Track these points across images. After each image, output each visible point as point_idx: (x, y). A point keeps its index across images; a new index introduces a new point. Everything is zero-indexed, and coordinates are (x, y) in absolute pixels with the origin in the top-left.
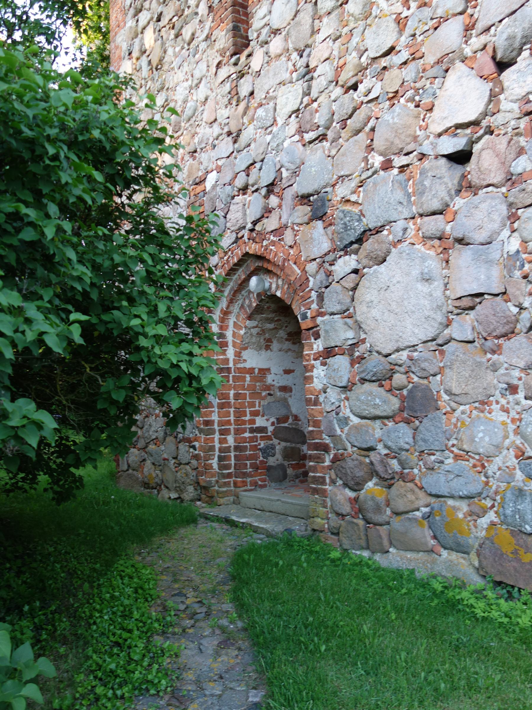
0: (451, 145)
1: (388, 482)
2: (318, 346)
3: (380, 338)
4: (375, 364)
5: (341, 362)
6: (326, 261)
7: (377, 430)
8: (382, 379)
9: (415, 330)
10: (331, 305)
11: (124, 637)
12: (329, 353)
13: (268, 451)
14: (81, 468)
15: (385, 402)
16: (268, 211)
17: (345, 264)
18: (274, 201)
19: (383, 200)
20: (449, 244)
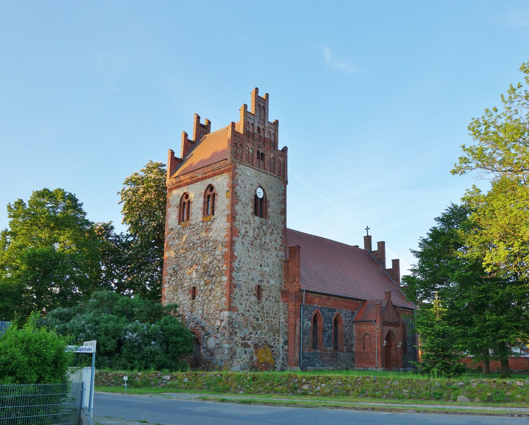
1: (209, 363)
5: (205, 349)
6: (204, 336)
7: (208, 357)
8: (209, 351)
9: (213, 346)
11: (484, 237)
12: (203, 348)
13: (193, 362)
16: (196, 326)
17: (206, 337)
19: (210, 331)
20: (216, 338)
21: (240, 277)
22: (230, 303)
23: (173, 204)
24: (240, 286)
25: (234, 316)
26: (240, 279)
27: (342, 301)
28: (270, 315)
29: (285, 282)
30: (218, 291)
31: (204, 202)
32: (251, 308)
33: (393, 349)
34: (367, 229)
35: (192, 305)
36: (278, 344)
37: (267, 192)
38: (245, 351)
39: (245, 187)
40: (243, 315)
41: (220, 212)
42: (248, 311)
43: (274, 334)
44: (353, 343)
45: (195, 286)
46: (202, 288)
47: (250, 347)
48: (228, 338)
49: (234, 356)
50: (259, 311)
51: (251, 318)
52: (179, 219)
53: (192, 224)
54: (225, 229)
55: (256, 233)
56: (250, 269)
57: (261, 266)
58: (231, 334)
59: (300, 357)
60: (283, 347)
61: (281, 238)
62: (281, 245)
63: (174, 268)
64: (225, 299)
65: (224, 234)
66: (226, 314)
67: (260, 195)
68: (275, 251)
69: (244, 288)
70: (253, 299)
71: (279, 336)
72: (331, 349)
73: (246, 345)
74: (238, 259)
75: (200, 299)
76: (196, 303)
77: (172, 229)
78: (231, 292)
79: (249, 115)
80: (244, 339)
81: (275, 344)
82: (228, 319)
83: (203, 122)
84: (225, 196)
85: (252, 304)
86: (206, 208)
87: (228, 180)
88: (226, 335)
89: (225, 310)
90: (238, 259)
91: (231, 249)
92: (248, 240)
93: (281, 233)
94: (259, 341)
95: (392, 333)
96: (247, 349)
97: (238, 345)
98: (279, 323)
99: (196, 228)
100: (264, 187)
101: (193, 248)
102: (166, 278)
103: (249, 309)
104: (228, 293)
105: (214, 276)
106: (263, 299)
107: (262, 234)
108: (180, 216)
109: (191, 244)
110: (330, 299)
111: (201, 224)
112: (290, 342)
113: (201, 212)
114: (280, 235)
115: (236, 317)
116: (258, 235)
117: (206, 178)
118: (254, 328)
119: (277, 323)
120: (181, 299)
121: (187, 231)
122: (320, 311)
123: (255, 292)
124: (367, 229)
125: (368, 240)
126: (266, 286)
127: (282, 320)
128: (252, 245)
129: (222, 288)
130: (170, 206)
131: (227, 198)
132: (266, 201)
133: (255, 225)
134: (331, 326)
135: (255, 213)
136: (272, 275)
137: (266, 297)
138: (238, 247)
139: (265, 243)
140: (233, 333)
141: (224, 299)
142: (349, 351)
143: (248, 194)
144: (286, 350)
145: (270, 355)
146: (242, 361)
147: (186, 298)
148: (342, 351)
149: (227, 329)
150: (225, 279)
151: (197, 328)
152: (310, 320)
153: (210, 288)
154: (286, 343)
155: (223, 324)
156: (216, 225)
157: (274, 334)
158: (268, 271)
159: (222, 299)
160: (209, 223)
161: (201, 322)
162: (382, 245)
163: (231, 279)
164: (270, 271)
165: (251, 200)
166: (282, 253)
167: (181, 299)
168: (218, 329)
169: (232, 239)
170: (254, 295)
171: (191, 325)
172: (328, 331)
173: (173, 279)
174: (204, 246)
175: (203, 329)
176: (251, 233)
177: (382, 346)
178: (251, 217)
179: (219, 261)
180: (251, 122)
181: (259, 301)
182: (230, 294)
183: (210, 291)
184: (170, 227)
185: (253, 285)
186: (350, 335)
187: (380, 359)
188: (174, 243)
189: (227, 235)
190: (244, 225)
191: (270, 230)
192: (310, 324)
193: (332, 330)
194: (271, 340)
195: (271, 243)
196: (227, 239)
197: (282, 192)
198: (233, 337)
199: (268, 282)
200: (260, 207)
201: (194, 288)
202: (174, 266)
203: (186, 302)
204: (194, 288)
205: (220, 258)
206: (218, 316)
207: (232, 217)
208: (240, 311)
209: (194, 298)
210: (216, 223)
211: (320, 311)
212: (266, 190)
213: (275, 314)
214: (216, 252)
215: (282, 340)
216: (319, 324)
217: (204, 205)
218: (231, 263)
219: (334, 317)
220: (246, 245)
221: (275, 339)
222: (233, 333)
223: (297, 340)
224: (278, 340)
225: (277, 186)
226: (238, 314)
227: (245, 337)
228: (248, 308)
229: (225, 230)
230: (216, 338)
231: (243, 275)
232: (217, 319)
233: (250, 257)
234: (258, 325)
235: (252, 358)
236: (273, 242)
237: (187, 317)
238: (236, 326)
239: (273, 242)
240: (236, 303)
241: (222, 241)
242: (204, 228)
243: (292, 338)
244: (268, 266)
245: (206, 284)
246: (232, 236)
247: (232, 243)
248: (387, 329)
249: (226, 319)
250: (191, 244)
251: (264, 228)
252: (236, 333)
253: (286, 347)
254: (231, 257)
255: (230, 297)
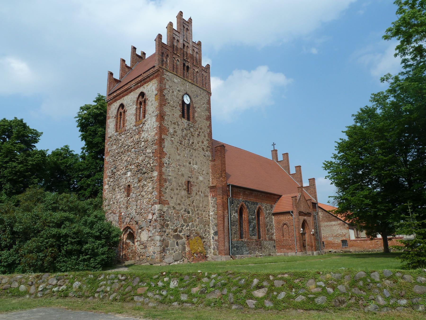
0: (149, 221)
2: (136, 240)
3: (142, 240)
4: (142, 243)
5: (139, 242)
8: (142, 244)
10: (138, 235)
12: (137, 241)
14: (79, 128)
15: (142, 247)
17: (140, 231)
18: (132, 220)
19: (143, 224)
20: (149, 231)
21: (170, 172)
22: (160, 197)
23: (111, 115)
24: (170, 181)
25: (165, 209)
26: (170, 174)
27: (262, 195)
28: (201, 209)
29: (212, 179)
30: (150, 186)
31: (137, 108)
32: (181, 202)
33: (307, 235)
34: (274, 145)
35: (127, 202)
36: (209, 235)
37: (193, 99)
38: (177, 243)
39: (173, 92)
40: (174, 208)
41: (150, 114)
42: (179, 204)
43: (205, 226)
44: (273, 232)
45: (129, 184)
46: (135, 185)
47: (182, 239)
48: (160, 230)
49: (166, 248)
50: (189, 205)
51: (182, 212)
52: (117, 128)
53: (127, 129)
54: (154, 128)
55: (184, 133)
56: (179, 165)
57: (190, 163)
58: (163, 227)
59: (229, 246)
60: (213, 237)
61: (207, 140)
62: (208, 147)
63: (112, 171)
64: (156, 193)
65: (153, 133)
66: (157, 207)
67: (187, 100)
68: (202, 151)
69: (174, 184)
70: (184, 193)
71: (209, 228)
72: (255, 237)
73: (178, 237)
74: (168, 156)
75: (134, 196)
76: (130, 200)
77: (110, 137)
78: (161, 186)
79: (174, 32)
80: (176, 231)
81: (205, 235)
82: (158, 212)
83: (138, 52)
84: (154, 99)
85: (182, 197)
86: (138, 114)
87: (156, 85)
88: (158, 228)
89: (155, 203)
90: (168, 156)
91: (161, 146)
92: (176, 139)
93: (207, 136)
94: (191, 233)
95: (306, 222)
96: (179, 241)
97: (170, 237)
98: (209, 215)
99: (131, 131)
100: (190, 94)
101: (128, 150)
102: (106, 180)
103: (179, 202)
104: (158, 187)
105: (146, 172)
106: (194, 193)
107: (190, 135)
108: (117, 125)
109: (126, 147)
110: (252, 193)
111: (134, 128)
112: (220, 233)
113: (134, 118)
114: (207, 138)
115: (167, 210)
116: (186, 135)
117: (138, 87)
118: (185, 221)
119: (207, 216)
120: (118, 197)
121: (123, 136)
122: (244, 204)
123: (185, 187)
124: (274, 145)
125: (275, 152)
126: (195, 181)
127: (211, 213)
128: (180, 143)
129: (153, 183)
130: (109, 118)
131: (156, 100)
132: (194, 108)
133: (183, 126)
134: (255, 218)
135: (183, 116)
136: (201, 172)
137: (195, 192)
138: (167, 143)
139: (193, 143)
140: (164, 226)
141: (156, 193)
142: (271, 239)
143: (175, 99)
144: (216, 240)
145: (201, 245)
146: (175, 252)
147: (122, 196)
148: (266, 240)
149: (159, 222)
150: (155, 174)
151: (131, 223)
152: (237, 212)
153: (142, 184)
154: (216, 233)
155: (155, 217)
156: (147, 126)
157: (205, 226)
158: (197, 169)
159: (153, 194)
160: (141, 125)
161: (135, 217)
162: (286, 155)
163: (161, 174)
164: (199, 168)
165: (178, 104)
166: (208, 153)
167: (118, 197)
168: (150, 222)
169: (161, 137)
170: (185, 190)
171: (126, 220)
172: (252, 222)
173: (111, 180)
174: (136, 147)
175: (137, 223)
176: (179, 132)
177: (299, 233)
178: (179, 119)
179: (150, 158)
180: (177, 38)
181: (189, 195)
182: (160, 188)
183: (142, 187)
184: (109, 136)
185: (184, 180)
186: (270, 225)
187: (298, 244)
188: (112, 149)
189: (156, 134)
190: (173, 126)
191: (197, 133)
192: (237, 215)
193: (255, 222)
194: (201, 232)
195: (198, 143)
196: (156, 137)
197: (206, 101)
198: (164, 229)
199: (197, 178)
200: (186, 111)
201: (129, 186)
202: (112, 169)
203: (122, 199)
204: (129, 186)
205: (151, 155)
206: (150, 209)
207: (161, 117)
208: (172, 205)
209: (128, 195)
210: (147, 125)
211: (244, 204)
212: (192, 96)
213: (205, 207)
214: (147, 151)
215: (212, 232)
216: (245, 216)
217: (137, 111)
218: (160, 158)
219: (257, 210)
220: (176, 143)
221: (205, 231)
222: (164, 226)
223: (226, 231)
224: (209, 232)
225: (202, 95)
226: (169, 208)
227: (177, 229)
228: (179, 202)
229: (155, 130)
230: (149, 231)
231: (172, 170)
232: (149, 212)
233: (179, 155)
234: (190, 218)
235: (184, 249)
236: (200, 144)
237: (123, 214)
238: (167, 218)
239: (200, 144)
240: (166, 197)
241: (153, 140)
242: (137, 131)
243: (221, 228)
244: (196, 164)
245: (139, 181)
246: (161, 135)
247: (161, 141)
248: (302, 218)
249: (157, 212)
250: (126, 147)
251: (192, 130)
252: (167, 225)
253: (216, 238)
254: (160, 153)
255: (160, 190)
